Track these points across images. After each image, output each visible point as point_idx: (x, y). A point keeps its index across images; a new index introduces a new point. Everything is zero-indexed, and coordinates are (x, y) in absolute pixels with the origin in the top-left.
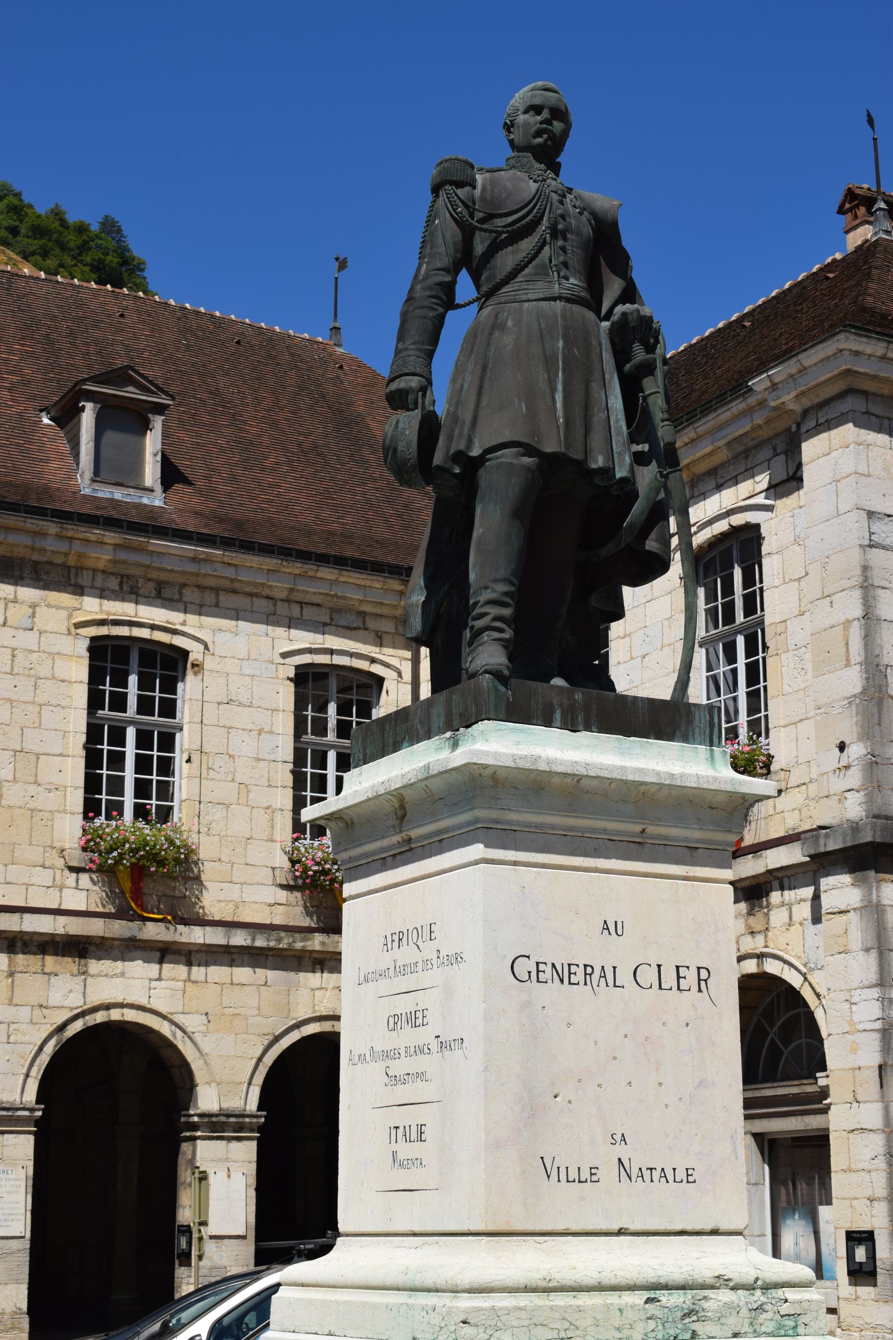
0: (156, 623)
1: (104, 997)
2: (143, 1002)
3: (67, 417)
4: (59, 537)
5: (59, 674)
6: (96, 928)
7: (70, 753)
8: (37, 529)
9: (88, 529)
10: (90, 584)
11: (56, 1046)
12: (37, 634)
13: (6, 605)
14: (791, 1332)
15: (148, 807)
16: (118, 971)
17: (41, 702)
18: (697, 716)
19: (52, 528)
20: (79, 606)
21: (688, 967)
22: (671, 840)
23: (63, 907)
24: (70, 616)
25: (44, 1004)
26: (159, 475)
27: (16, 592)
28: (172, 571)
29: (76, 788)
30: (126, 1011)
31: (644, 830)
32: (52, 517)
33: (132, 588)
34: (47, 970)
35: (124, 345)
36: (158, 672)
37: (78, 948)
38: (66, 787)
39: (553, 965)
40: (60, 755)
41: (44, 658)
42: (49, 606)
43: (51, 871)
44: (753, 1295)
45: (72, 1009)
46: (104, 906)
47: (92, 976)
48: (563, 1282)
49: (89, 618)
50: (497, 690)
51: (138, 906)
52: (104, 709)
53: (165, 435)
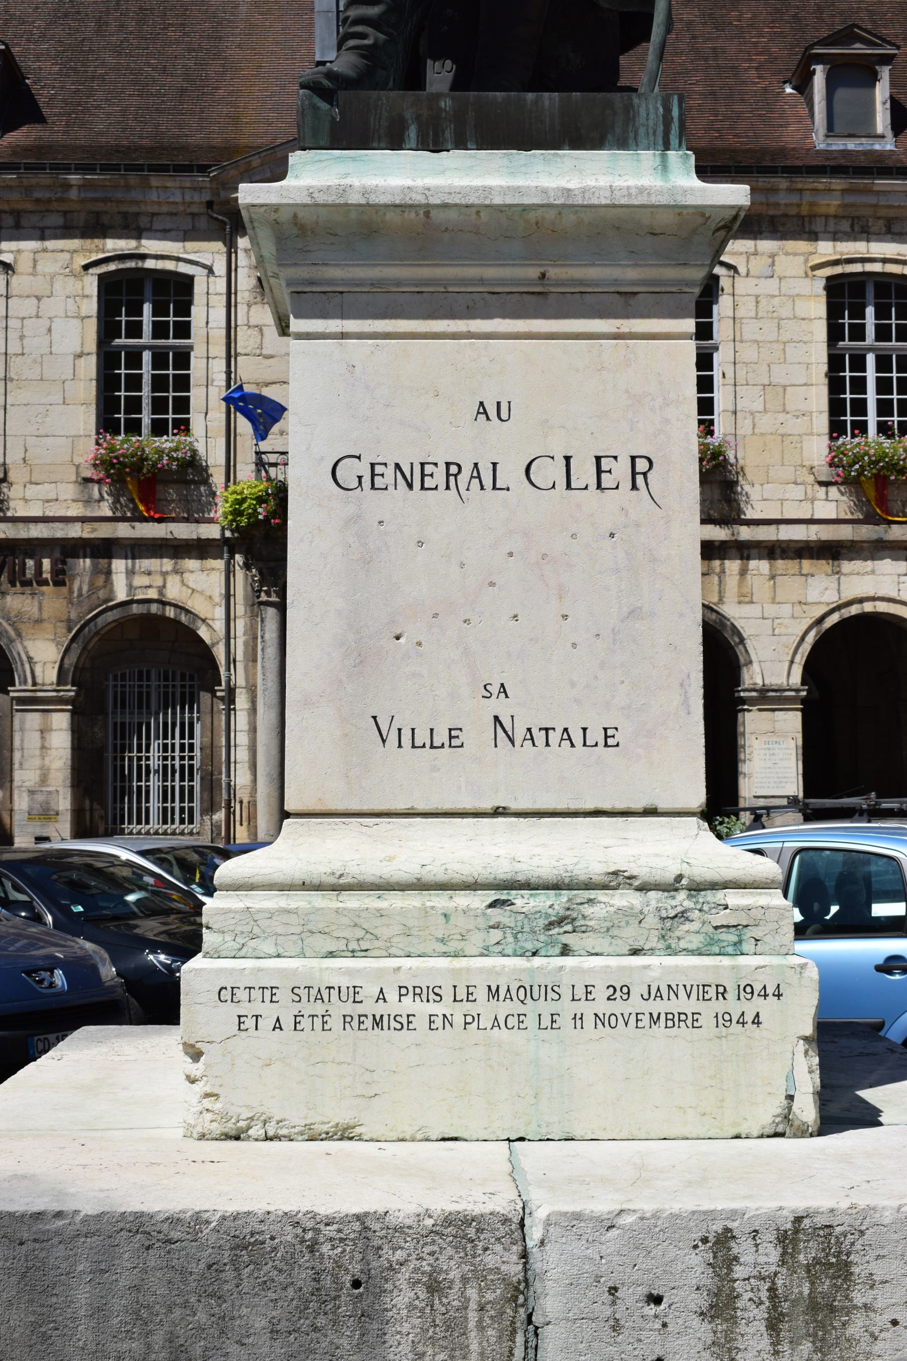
0: (887, 256)
1: (857, 593)
2: (893, 594)
3: (804, 85)
4: (790, 190)
5: (800, 313)
6: (845, 533)
7: (814, 382)
8: (769, 186)
9: (815, 180)
10: (823, 229)
11: (816, 636)
12: (778, 280)
13: (748, 258)
14: (730, 950)
15: (890, 423)
16: (869, 569)
17: (785, 340)
18: (642, 111)
19: (783, 183)
20: (814, 251)
21: (615, 458)
22: (589, 285)
23: (816, 517)
24: (807, 261)
25: (803, 601)
26: (889, 121)
27: (756, 246)
28: (899, 207)
29: (821, 412)
30: (878, 603)
31: (543, 276)
32: (782, 173)
33: (862, 227)
34: (804, 572)
35: (868, 11)
36: (894, 301)
37: (831, 552)
38: (811, 413)
39: (397, 466)
40: (805, 385)
41: (785, 301)
42: (787, 254)
43: (802, 487)
44: (673, 898)
45: (828, 604)
46: (852, 513)
47: (845, 575)
48: (361, 878)
49: (824, 260)
50: (315, 108)
51: (883, 511)
52: (844, 340)
53: (893, 85)
